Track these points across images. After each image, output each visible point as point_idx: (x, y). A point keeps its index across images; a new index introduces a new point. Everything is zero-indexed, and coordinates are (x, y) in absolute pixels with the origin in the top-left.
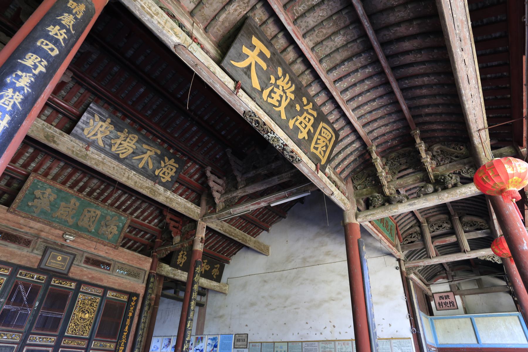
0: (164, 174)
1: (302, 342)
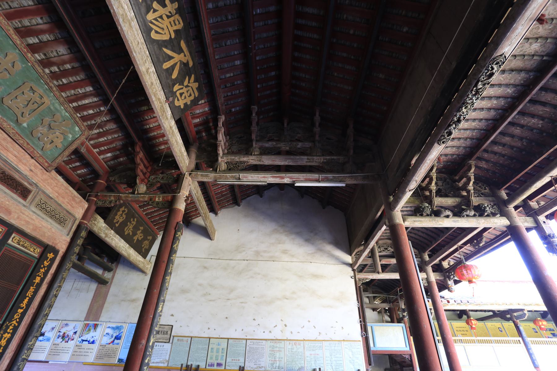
0: (181, 94)
1: (246, 339)
